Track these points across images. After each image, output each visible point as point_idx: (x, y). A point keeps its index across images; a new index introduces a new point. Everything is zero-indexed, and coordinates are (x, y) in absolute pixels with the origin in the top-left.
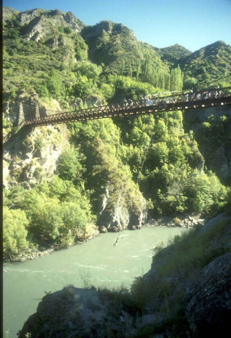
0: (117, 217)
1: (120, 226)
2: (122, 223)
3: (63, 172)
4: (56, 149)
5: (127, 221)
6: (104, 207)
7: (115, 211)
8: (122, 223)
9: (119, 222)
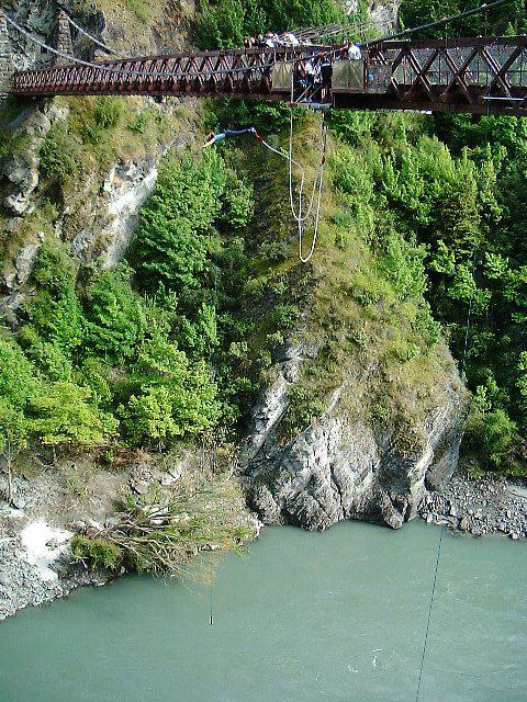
0: (318, 460)
2: (338, 484)
3: (147, 260)
4: (129, 173)
6: (273, 417)
7: (313, 435)
8: (338, 484)
9: (326, 481)
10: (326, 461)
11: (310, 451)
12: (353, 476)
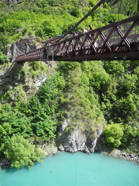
1: (75, 147)
2: (77, 145)
5: (82, 143)
10: (74, 140)
11: (71, 137)
12: (80, 143)
